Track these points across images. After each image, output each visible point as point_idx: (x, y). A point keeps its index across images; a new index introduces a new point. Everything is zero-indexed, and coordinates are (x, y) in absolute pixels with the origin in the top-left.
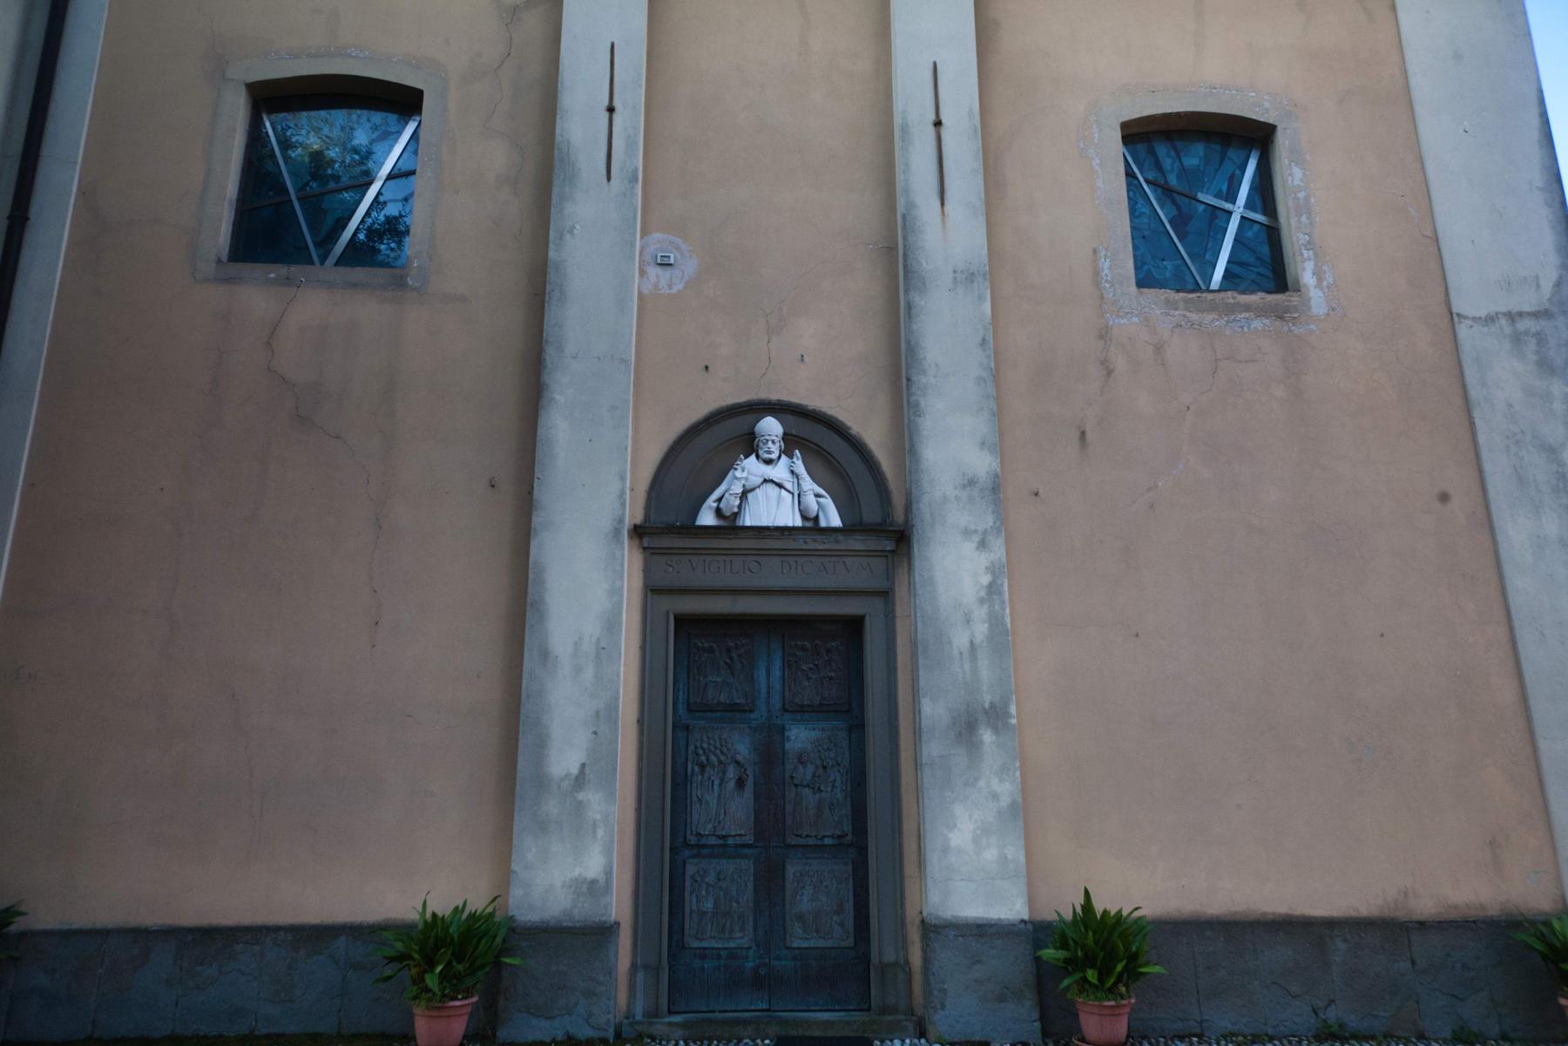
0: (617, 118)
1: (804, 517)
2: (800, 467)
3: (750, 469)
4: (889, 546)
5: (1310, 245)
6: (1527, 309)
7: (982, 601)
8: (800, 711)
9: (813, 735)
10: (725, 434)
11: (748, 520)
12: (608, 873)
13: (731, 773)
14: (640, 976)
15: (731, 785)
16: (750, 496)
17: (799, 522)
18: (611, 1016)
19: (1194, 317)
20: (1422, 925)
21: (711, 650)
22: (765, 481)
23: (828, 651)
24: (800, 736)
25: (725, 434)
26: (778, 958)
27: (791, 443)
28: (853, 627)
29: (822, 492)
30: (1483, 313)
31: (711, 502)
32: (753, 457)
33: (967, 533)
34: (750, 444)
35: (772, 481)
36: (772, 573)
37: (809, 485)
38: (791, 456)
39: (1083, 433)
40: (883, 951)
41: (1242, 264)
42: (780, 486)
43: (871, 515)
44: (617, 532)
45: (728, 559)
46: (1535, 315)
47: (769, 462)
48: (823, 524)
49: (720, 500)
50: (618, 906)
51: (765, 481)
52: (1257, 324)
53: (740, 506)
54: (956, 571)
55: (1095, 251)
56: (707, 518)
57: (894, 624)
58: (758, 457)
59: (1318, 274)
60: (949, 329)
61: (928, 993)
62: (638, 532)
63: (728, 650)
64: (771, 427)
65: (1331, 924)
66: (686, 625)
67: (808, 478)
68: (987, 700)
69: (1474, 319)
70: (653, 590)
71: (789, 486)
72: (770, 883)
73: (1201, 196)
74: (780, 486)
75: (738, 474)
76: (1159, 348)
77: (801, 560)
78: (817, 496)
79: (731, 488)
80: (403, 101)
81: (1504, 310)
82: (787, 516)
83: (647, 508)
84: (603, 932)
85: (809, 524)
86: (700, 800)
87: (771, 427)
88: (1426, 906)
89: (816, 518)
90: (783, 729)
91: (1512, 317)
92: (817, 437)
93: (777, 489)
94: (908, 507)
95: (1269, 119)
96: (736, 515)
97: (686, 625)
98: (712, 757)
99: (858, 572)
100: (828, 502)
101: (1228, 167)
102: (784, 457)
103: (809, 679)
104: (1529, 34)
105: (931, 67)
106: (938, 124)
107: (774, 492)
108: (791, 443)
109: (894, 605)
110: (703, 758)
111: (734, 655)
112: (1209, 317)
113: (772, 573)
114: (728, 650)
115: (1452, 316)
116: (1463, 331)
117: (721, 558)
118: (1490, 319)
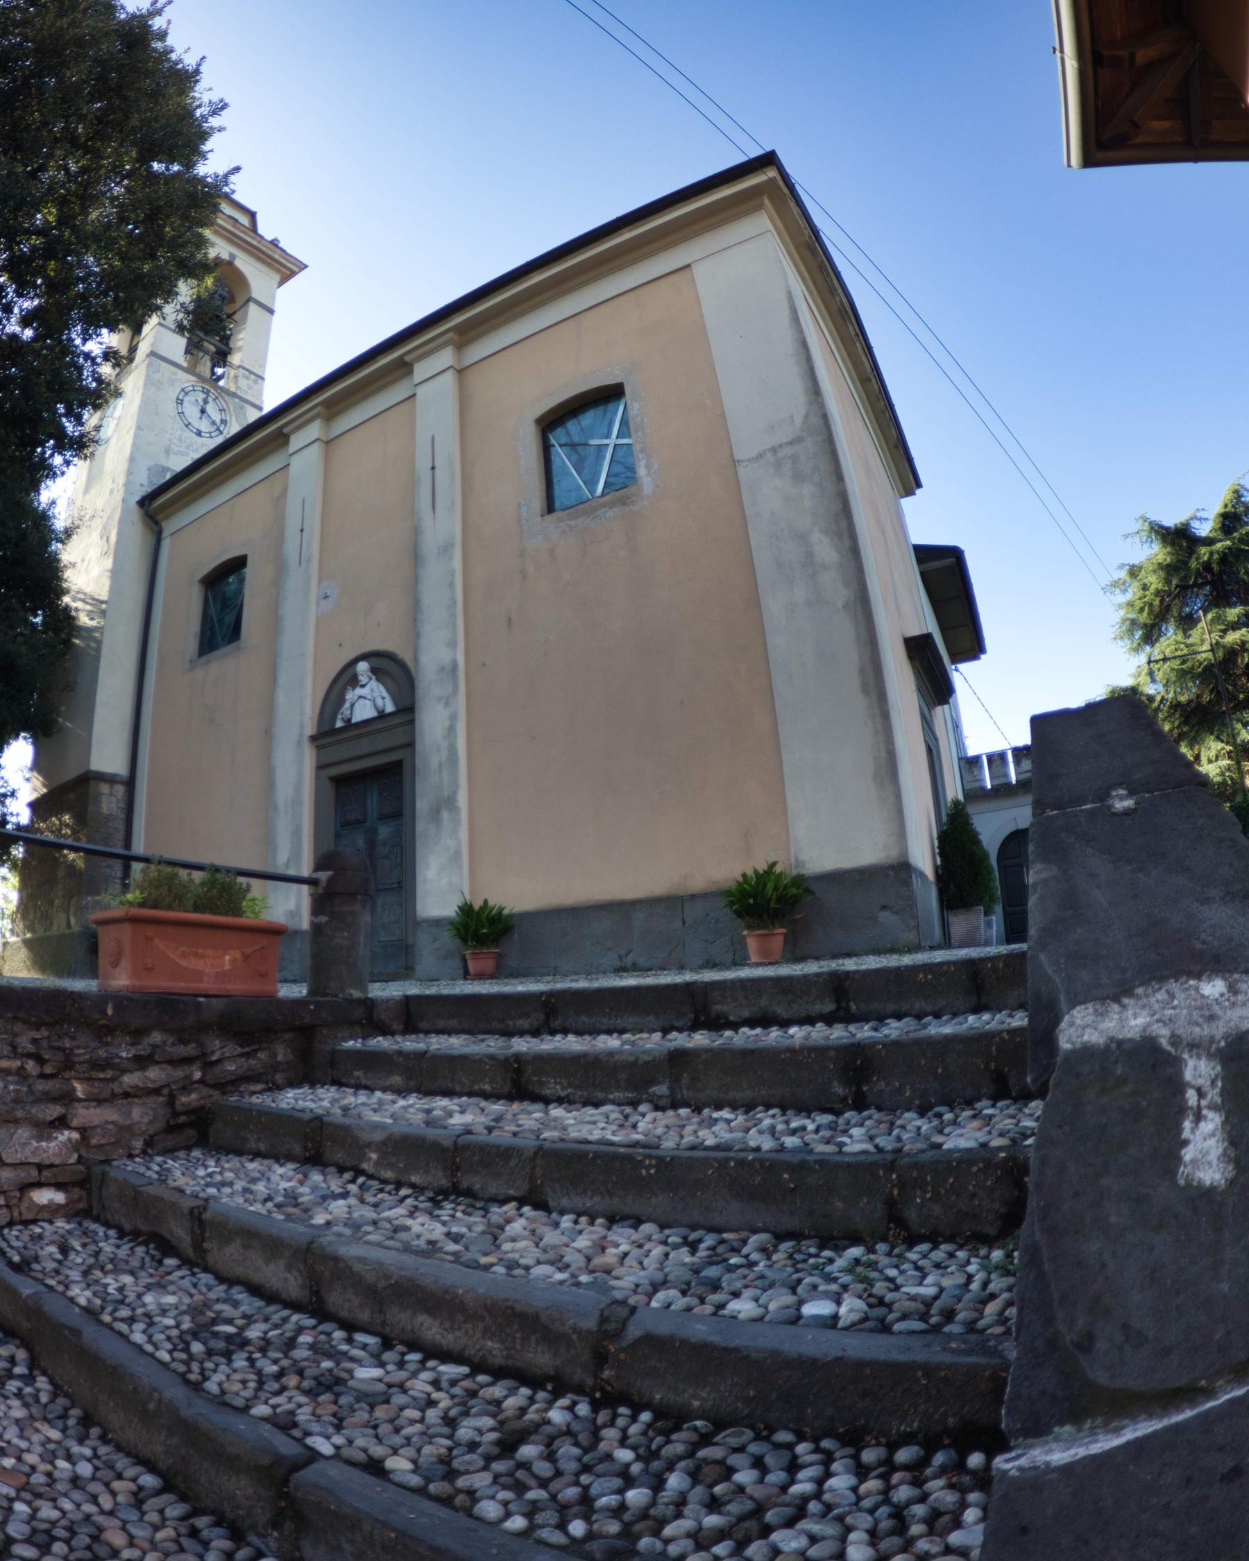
0: (437, 472)
5: (642, 451)
6: (785, 440)
7: (445, 737)
11: (353, 721)
19: (572, 523)
20: (693, 897)
25: (347, 678)
30: (754, 454)
33: (440, 699)
36: (366, 746)
39: (510, 620)
41: (616, 475)
44: (299, 743)
46: (791, 443)
52: (610, 514)
54: (434, 722)
55: (519, 504)
56: (339, 724)
59: (648, 467)
60: (442, 581)
62: (313, 738)
64: (363, 666)
65: (635, 903)
68: (446, 794)
69: (749, 460)
70: (320, 767)
73: (592, 442)
76: (552, 551)
80: (610, 394)
81: (768, 446)
82: (371, 713)
88: (698, 884)
91: (774, 450)
95: (619, 381)
97: (340, 782)
99: (398, 738)
101: (609, 415)
105: (429, 440)
106: (433, 468)
108: (374, 671)
112: (581, 520)
115: (735, 463)
116: (741, 471)
118: (760, 456)
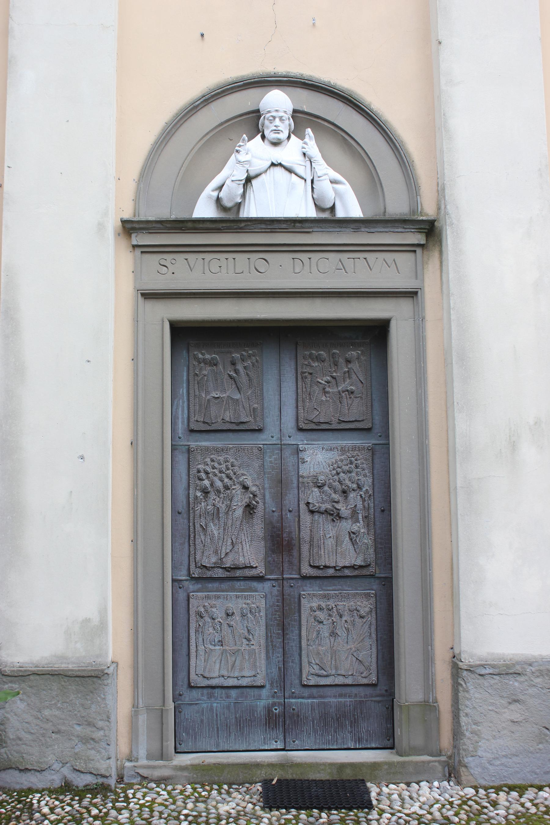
1: (319, 208)
2: (313, 149)
3: (254, 152)
4: (420, 239)
8: (312, 429)
9: (335, 456)
10: (231, 110)
11: (252, 210)
12: (103, 612)
13: (240, 500)
14: (143, 718)
15: (239, 512)
16: (254, 182)
17: (311, 213)
18: (112, 762)
21: (213, 363)
22: (273, 165)
23: (348, 361)
24: (319, 458)
26: (293, 696)
27: (301, 120)
28: (376, 334)
29: (337, 176)
31: (209, 191)
32: (259, 137)
34: (253, 122)
35: (280, 165)
36: (282, 272)
37: (323, 169)
38: (302, 137)
40: (409, 689)
42: (290, 170)
43: (396, 205)
45: (230, 256)
47: (276, 144)
48: (340, 214)
49: (220, 188)
50: (115, 648)
51: (273, 165)
53: (244, 195)
57: (424, 329)
58: (263, 137)
61: (457, 733)
62: (129, 228)
63: (233, 364)
66: (183, 334)
67: (322, 162)
71: (300, 170)
72: (284, 622)
74: (290, 170)
75: (242, 157)
77: (315, 257)
78: (333, 182)
79: (231, 173)
83: (137, 200)
84: (89, 679)
85: (326, 215)
86: (204, 530)
87: (278, 103)
89: (333, 209)
90: (298, 451)
92: (332, 112)
93: (287, 173)
94: (441, 192)
96: (238, 206)
97: (183, 334)
98: (216, 479)
100: (346, 189)
102: (293, 137)
103: (325, 393)
104: (394, 676)
107: (284, 177)
109: (423, 309)
110: (206, 483)
111: (240, 367)
113: (282, 272)
114: (233, 364)
117: (223, 256)
